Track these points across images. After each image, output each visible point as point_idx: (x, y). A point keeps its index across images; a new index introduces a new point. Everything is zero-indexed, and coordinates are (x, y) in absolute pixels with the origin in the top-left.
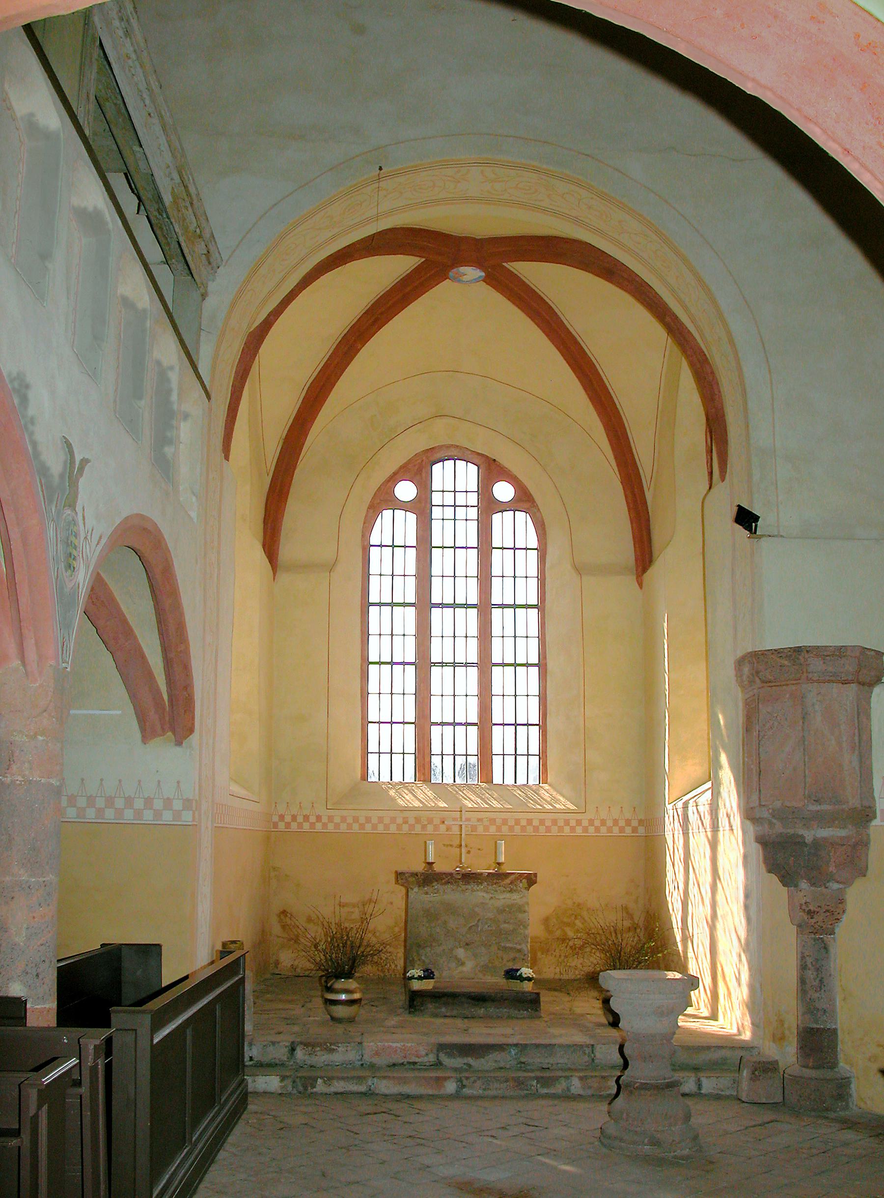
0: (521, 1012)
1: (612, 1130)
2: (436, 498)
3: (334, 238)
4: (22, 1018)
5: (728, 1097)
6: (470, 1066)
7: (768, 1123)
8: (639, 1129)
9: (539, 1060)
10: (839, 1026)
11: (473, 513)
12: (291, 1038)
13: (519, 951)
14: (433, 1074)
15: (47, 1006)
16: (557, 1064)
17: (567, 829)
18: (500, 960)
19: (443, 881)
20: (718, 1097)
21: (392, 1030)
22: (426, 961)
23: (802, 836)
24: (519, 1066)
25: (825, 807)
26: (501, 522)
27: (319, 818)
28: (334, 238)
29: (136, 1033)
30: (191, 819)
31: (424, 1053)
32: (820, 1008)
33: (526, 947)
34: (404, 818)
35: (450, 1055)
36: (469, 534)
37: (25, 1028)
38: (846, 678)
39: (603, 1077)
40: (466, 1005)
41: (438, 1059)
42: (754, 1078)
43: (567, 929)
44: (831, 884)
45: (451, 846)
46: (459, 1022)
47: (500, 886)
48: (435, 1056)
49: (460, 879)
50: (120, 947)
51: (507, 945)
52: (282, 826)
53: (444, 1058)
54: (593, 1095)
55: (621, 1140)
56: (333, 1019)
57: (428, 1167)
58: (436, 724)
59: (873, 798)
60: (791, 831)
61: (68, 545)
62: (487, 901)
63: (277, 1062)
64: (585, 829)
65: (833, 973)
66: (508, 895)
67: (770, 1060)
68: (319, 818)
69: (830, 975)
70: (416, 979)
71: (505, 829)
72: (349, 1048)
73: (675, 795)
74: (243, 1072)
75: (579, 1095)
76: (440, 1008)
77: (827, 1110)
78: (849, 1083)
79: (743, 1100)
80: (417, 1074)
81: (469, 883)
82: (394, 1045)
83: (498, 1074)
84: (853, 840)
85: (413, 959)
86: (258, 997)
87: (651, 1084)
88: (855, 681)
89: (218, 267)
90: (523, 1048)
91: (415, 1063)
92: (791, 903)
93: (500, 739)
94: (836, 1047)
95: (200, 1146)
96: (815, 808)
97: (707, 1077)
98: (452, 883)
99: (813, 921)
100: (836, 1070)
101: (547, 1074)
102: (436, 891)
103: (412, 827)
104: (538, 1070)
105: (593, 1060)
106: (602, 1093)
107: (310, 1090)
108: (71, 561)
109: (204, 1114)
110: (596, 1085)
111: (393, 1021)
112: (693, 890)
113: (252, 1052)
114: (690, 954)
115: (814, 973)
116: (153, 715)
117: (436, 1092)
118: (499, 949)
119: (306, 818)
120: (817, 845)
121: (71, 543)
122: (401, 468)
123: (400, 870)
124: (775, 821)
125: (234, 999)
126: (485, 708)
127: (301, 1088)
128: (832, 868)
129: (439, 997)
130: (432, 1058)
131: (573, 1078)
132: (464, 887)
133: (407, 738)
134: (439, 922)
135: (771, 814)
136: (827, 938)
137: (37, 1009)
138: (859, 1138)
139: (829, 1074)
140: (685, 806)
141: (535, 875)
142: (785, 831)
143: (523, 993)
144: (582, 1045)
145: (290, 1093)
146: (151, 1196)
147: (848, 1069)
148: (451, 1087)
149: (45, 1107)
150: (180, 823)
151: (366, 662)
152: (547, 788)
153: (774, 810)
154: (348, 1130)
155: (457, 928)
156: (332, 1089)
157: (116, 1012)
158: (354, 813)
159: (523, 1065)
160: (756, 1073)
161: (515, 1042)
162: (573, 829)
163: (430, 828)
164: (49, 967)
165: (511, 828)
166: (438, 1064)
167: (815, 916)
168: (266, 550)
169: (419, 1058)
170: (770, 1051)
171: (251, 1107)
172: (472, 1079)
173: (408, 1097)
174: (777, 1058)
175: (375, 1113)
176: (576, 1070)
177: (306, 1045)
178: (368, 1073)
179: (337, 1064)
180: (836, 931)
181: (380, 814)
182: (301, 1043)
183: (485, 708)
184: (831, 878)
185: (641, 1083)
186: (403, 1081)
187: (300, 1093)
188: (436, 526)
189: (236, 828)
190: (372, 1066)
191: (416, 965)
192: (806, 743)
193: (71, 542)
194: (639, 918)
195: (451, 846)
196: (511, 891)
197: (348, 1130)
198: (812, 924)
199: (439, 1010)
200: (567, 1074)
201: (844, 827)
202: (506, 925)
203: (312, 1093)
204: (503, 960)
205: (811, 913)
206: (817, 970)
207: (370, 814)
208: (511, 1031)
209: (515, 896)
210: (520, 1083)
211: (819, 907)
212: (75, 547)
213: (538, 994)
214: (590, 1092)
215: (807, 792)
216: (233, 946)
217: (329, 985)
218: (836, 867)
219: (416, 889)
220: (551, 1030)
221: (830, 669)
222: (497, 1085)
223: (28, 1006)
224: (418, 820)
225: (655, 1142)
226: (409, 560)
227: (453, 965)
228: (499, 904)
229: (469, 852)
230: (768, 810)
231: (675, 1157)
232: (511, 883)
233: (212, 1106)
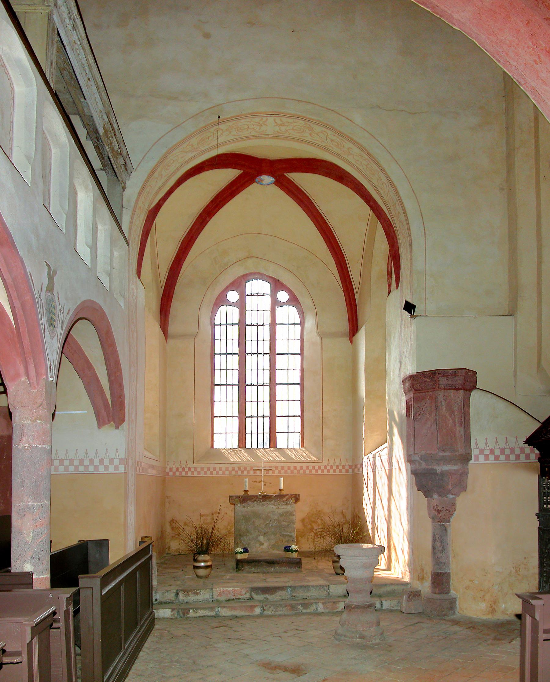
0: (292, 569)
1: (340, 631)
3: (194, 158)
4: (30, 584)
5: (396, 610)
6: (266, 598)
7: (416, 623)
8: (354, 630)
9: (302, 594)
10: (451, 571)
12: (177, 588)
13: (291, 536)
14: (249, 604)
15: (45, 576)
16: (311, 596)
17: (313, 471)
18: (281, 542)
19: (253, 500)
20: (391, 611)
21: (229, 581)
22: (244, 543)
23: (436, 470)
24: (292, 598)
25: (447, 454)
27: (190, 469)
28: (194, 158)
29: (92, 590)
30: (124, 470)
31: (244, 593)
32: (442, 562)
33: (294, 534)
34: (232, 467)
35: (257, 594)
37: (32, 590)
39: (334, 602)
40: (265, 566)
41: (251, 596)
42: (409, 600)
43: (314, 525)
44: (449, 495)
45: (256, 482)
46: (261, 576)
47: (281, 502)
48: (250, 595)
49: (261, 499)
50: (87, 542)
51: (285, 533)
52: (171, 474)
53: (255, 596)
54: (329, 612)
55: (345, 636)
56: (197, 576)
57: (248, 655)
58: (248, 417)
59: (471, 449)
60: (430, 467)
61: (50, 313)
63: (170, 601)
64: (323, 471)
66: (285, 506)
67: (417, 590)
69: (448, 544)
70: (239, 553)
71: (283, 472)
72: (206, 592)
73: (368, 451)
74: (152, 607)
75: (322, 612)
76: (251, 568)
77: (445, 615)
78: (456, 601)
79: (403, 612)
80: (240, 604)
81: (266, 501)
82: (229, 589)
83: (282, 603)
84: (461, 471)
85: (238, 543)
86: (159, 567)
87: (361, 606)
90: (294, 588)
91: (239, 599)
92: (429, 507)
93: (281, 423)
94: (449, 582)
95: (130, 650)
96: (441, 454)
97: (386, 600)
98: (257, 501)
99: (440, 515)
100: (449, 594)
101: (306, 602)
102: (249, 506)
103: (236, 472)
104: (301, 600)
105: (329, 593)
106: (334, 611)
107: (186, 616)
108: (52, 322)
109: (131, 633)
110: (330, 607)
111: (228, 576)
112: (378, 503)
113: (157, 596)
114: (376, 536)
116: (103, 413)
117: (251, 614)
118: (280, 536)
119: (183, 469)
120: (443, 474)
121: (52, 312)
123: (231, 495)
124: (421, 462)
125: (146, 568)
126: (273, 408)
127: (182, 615)
128: (450, 487)
129: (251, 562)
130: (248, 595)
131: (319, 603)
132: (263, 503)
133: (233, 424)
134: (251, 522)
135: (420, 458)
136: (447, 524)
137: (39, 578)
138: (461, 629)
139: (445, 596)
140: (374, 457)
141: (299, 495)
142: (427, 467)
143: (293, 559)
144: (323, 586)
145: (176, 618)
146: (103, 680)
147: (455, 593)
148: (258, 611)
149: (36, 638)
150: (118, 472)
151: (213, 385)
152: (303, 450)
153: (421, 456)
154: (206, 637)
156: (198, 615)
157: (82, 578)
158: (208, 466)
159: (294, 597)
160: (410, 597)
161: (290, 585)
162: (316, 471)
163: (246, 472)
164: (46, 554)
165: (286, 471)
166: (251, 598)
167: (441, 513)
168: (162, 328)
169: (241, 596)
170: (418, 586)
171: (156, 627)
172: (269, 606)
173: (236, 617)
174: (420, 589)
175: (220, 627)
176: (320, 599)
177: (184, 591)
178: (214, 605)
179: (200, 601)
180: (451, 521)
181: (221, 465)
182: (181, 590)
183: (273, 408)
184: (449, 492)
185: (355, 605)
186: (234, 609)
187: (181, 617)
189: (147, 475)
190: (218, 601)
191: (239, 546)
192: (438, 422)
193: (52, 311)
194: (349, 517)
195: (256, 482)
196: (287, 504)
197: (206, 637)
198: (440, 517)
199: (251, 570)
200: (316, 601)
201: (456, 464)
202: (284, 523)
203: (188, 617)
204: (282, 541)
205: (439, 511)
206: (441, 542)
208: (288, 580)
209: (289, 507)
210: (292, 607)
212: (54, 314)
213: (300, 559)
214: (327, 611)
215: (438, 446)
216: (146, 539)
217: (195, 558)
218: (452, 486)
219: (239, 505)
220: (307, 578)
221: (450, 382)
222: (281, 609)
223: (34, 577)
224: (239, 468)
225: (362, 637)
228: (280, 511)
229: (265, 485)
230: (418, 456)
231: (373, 644)
232: (286, 500)
233: (136, 627)
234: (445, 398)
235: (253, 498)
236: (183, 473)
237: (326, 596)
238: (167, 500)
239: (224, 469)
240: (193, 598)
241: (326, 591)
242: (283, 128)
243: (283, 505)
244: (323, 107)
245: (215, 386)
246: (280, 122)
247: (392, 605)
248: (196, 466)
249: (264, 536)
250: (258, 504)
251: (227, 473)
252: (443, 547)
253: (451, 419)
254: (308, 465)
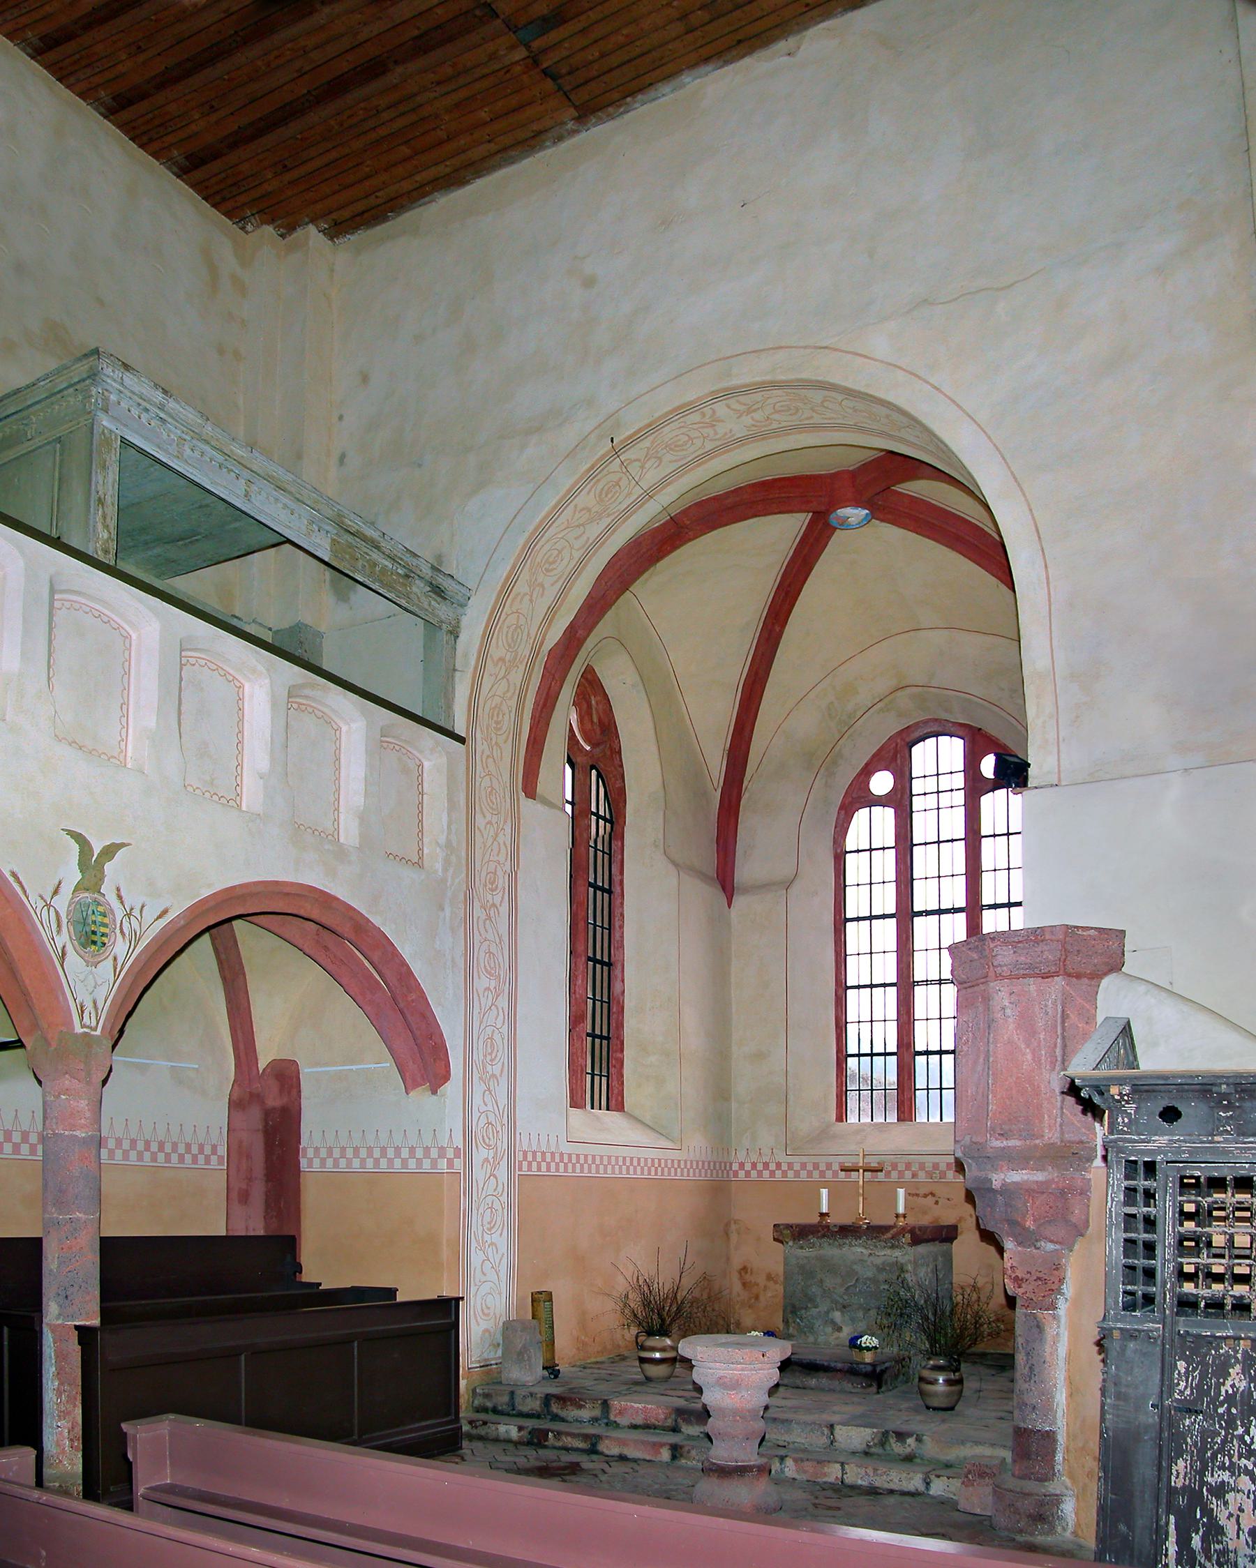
2: (917, 786)
3: (610, 529)
9: (775, 1437)
11: (959, 798)
19: (819, 1234)
25: (1012, 1143)
27: (779, 1165)
36: (955, 824)
38: (1046, 971)
40: (797, 1374)
45: (917, 1195)
47: (880, 1241)
49: (836, 1232)
52: (742, 1174)
62: (866, 1258)
65: (1048, 1359)
66: (888, 1252)
68: (779, 1165)
88: (1061, 972)
89: (469, 598)
106: (819, 1480)
115: (1025, 1358)
122: (874, 756)
130: (669, 1423)
131: (787, 1459)
134: (816, 1280)
155: (834, 1288)
158: (815, 1159)
167: (1023, 1285)
192: (991, 1059)
195: (917, 1195)
196: (893, 1247)
201: (1043, 1169)
207: (831, 1159)
211: (1028, 1272)
218: (1034, 1221)
219: (791, 1243)
221: (1022, 959)
226: (887, 864)
227: (829, 1329)
228: (879, 1261)
232: (892, 1238)
234: (1014, 998)
236: (766, 1174)
237: (825, 1448)
238: (733, 1227)
240: (572, 1414)
241: (825, 1437)
242: (758, 416)
243: (885, 1247)
244: (805, 347)
245: (848, 991)
246: (742, 408)
247: (952, 1489)
248: (790, 1159)
249: (842, 1313)
250: (830, 1244)
252: (1030, 1368)
253: (1028, 1050)
254: (895, 1161)
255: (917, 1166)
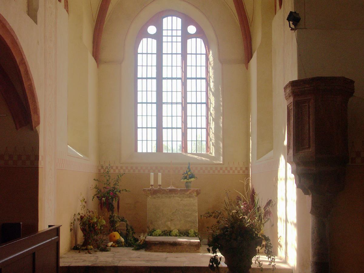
2: (165, 33)
11: (179, 39)
26: (191, 43)
36: (178, 48)
66: (188, 199)
141: (200, 190)
188: (164, 45)
196: (190, 197)
219: (150, 196)
235: (162, 191)
239: (124, 168)
251: (221, 172)
255: (115, 167)
